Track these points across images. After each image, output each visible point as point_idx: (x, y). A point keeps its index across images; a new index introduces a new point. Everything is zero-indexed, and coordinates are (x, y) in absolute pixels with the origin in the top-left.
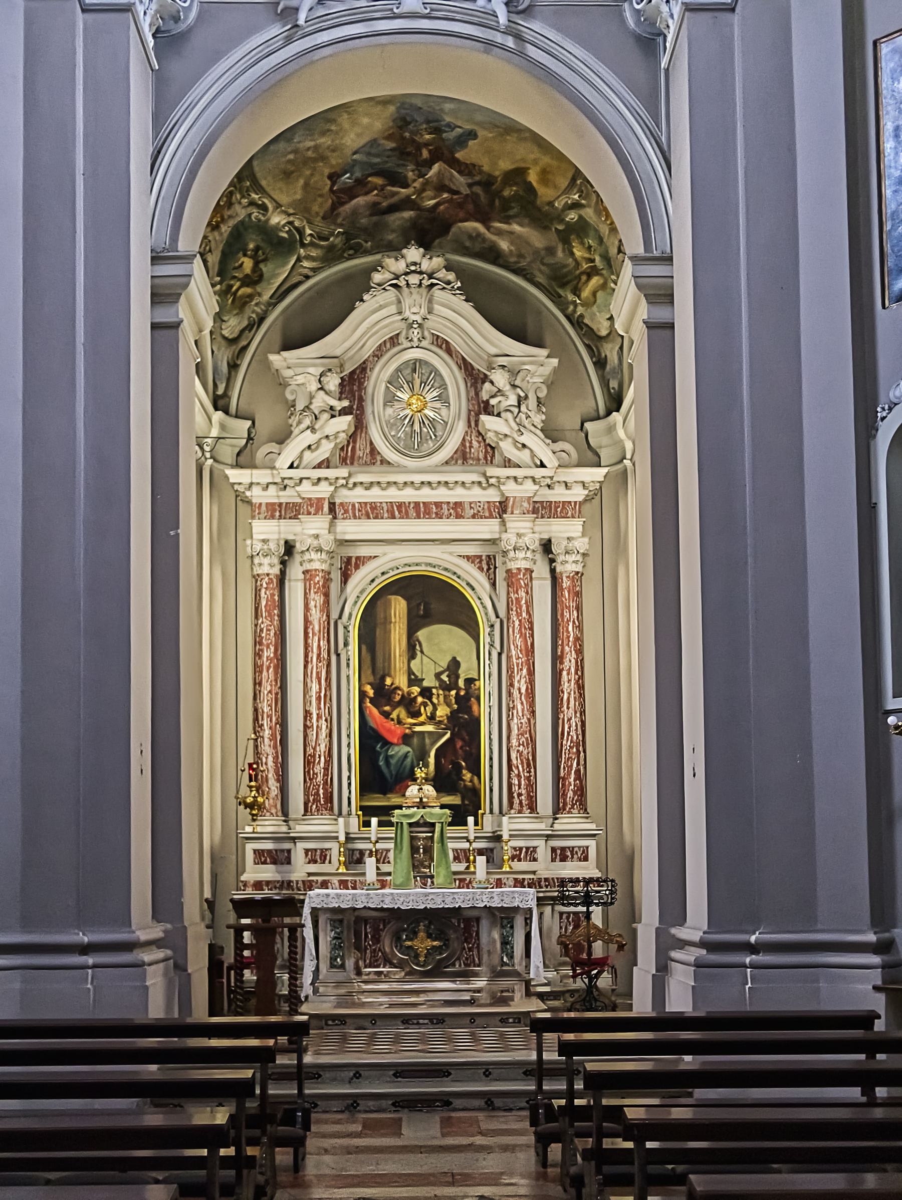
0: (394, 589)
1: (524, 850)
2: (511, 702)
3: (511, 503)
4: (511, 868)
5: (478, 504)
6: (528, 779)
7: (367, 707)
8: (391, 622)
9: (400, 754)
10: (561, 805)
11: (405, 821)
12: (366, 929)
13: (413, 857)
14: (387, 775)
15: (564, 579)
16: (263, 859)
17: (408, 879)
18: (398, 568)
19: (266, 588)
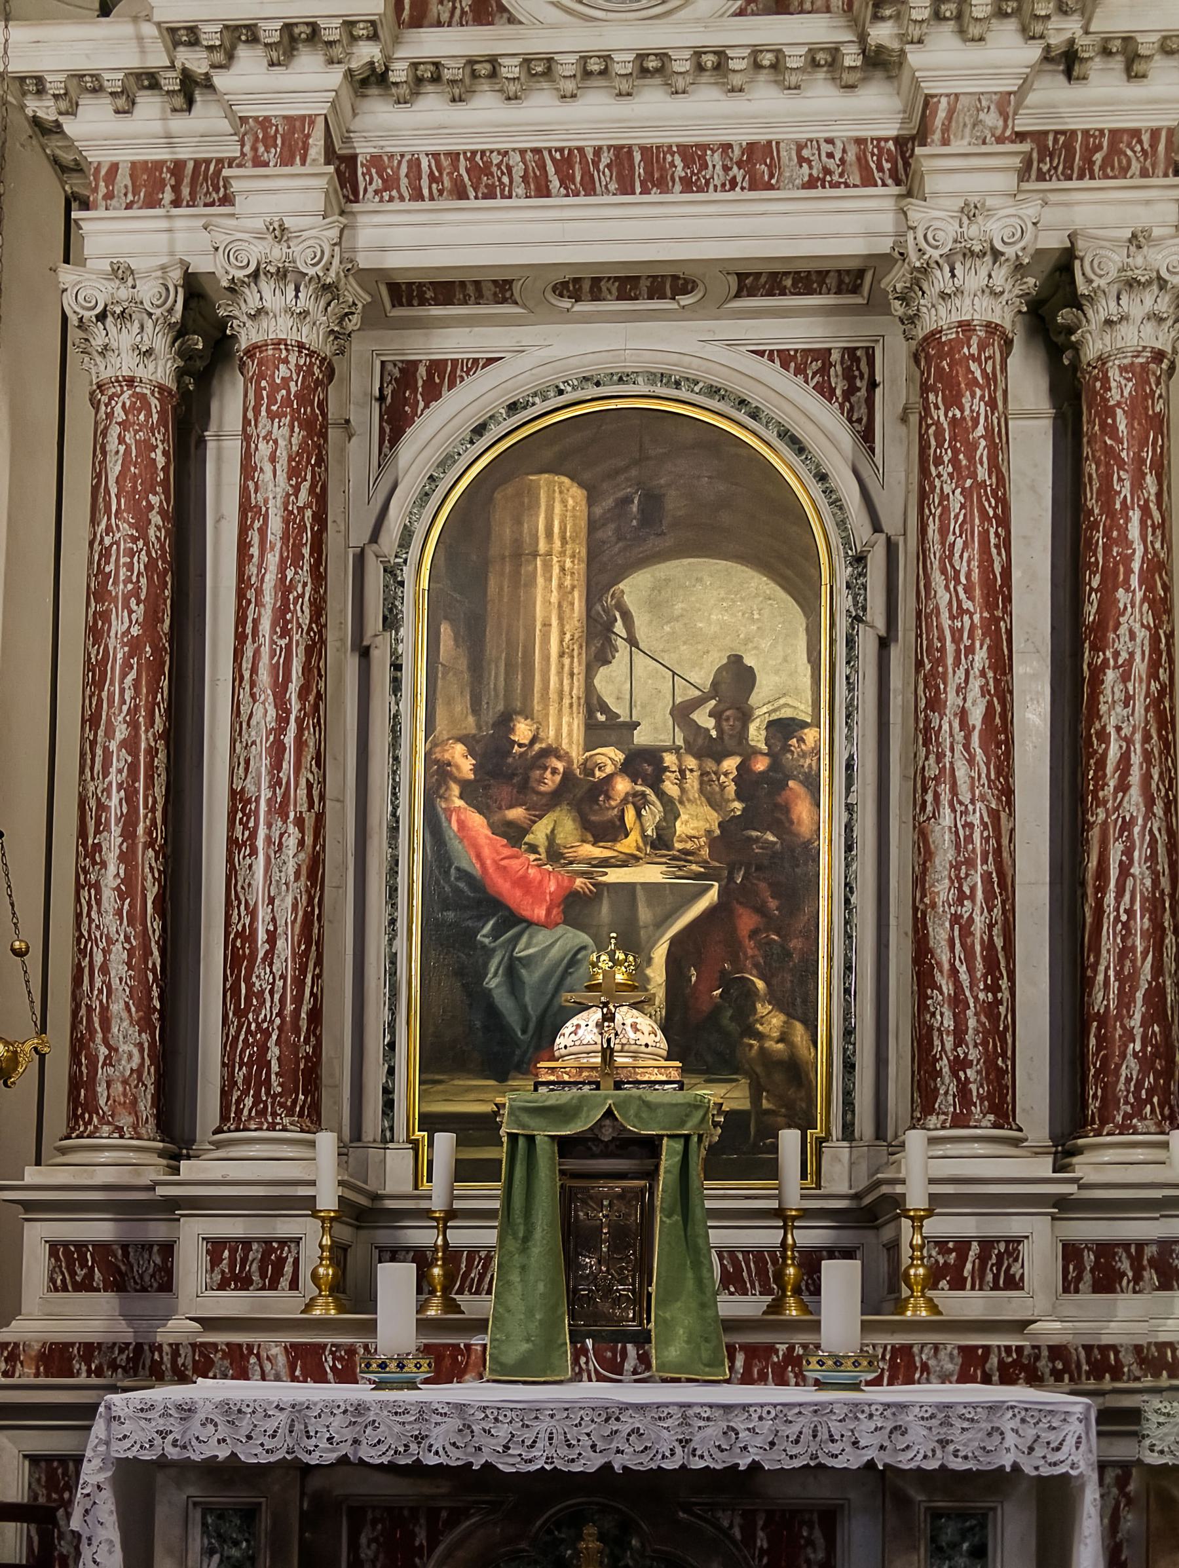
0: (548, 454)
1: (975, 1248)
2: (932, 758)
3: (942, 114)
4: (933, 1308)
5: (829, 148)
6: (990, 1010)
7: (449, 811)
8: (535, 554)
9: (555, 953)
10: (1093, 1106)
11: (544, 1132)
12: (354, 1546)
13: (571, 1264)
14: (513, 1019)
15: (1114, 374)
16: (81, 1273)
17: (550, 1344)
18: (561, 392)
19: (124, 425)
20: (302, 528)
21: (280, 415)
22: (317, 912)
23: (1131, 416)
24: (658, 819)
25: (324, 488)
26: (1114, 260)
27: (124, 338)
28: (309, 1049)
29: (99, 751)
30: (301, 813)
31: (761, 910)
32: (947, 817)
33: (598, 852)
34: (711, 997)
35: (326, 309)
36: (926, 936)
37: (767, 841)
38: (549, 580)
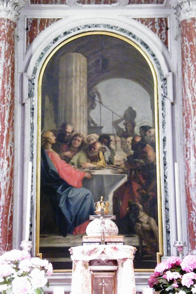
14: (68, 217)
18: (79, 29)
22: (12, 186)
24: (109, 155)
25: (14, 60)
28: (10, 229)
30: (8, 156)
31: (140, 183)
34: (126, 210)
35: (14, 9)
36: (189, 194)
37: (141, 162)
38: (76, 84)
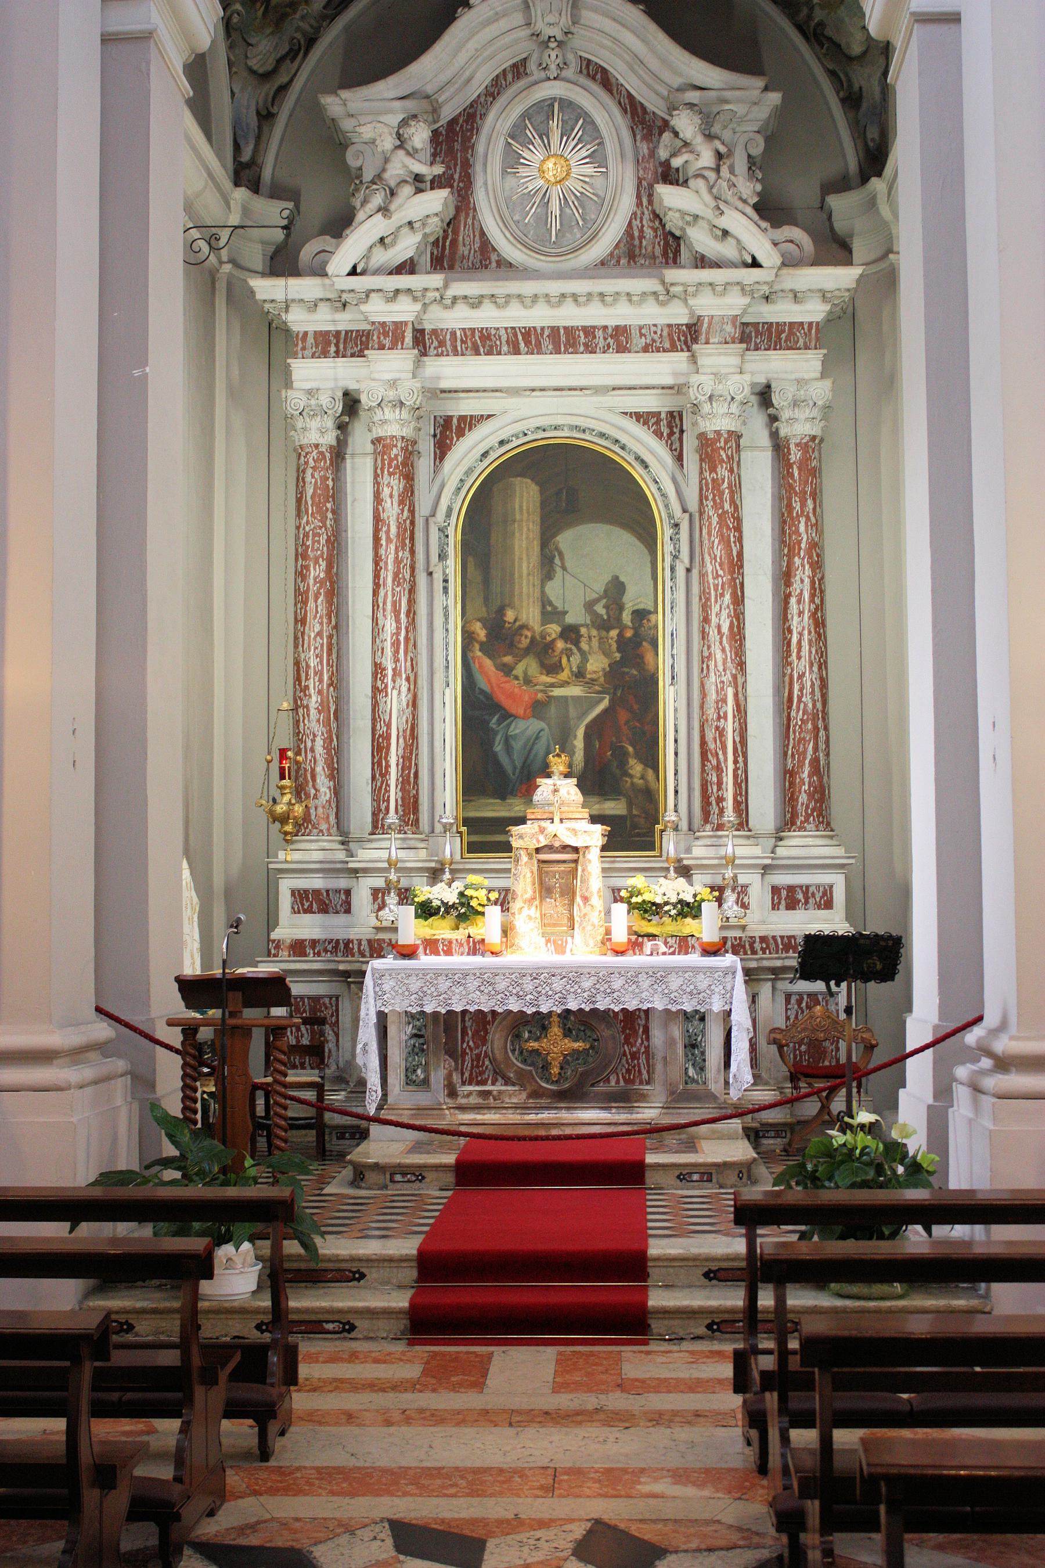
2: (706, 648)
7: (473, 658)
8: (514, 521)
15: (792, 446)
16: (306, 905)
18: (526, 435)
19: (314, 468)
20: (405, 530)
21: (394, 474)
23: (800, 469)
26: (791, 391)
27: (314, 424)
29: (306, 638)
32: (713, 677)
33: (549, 680)
